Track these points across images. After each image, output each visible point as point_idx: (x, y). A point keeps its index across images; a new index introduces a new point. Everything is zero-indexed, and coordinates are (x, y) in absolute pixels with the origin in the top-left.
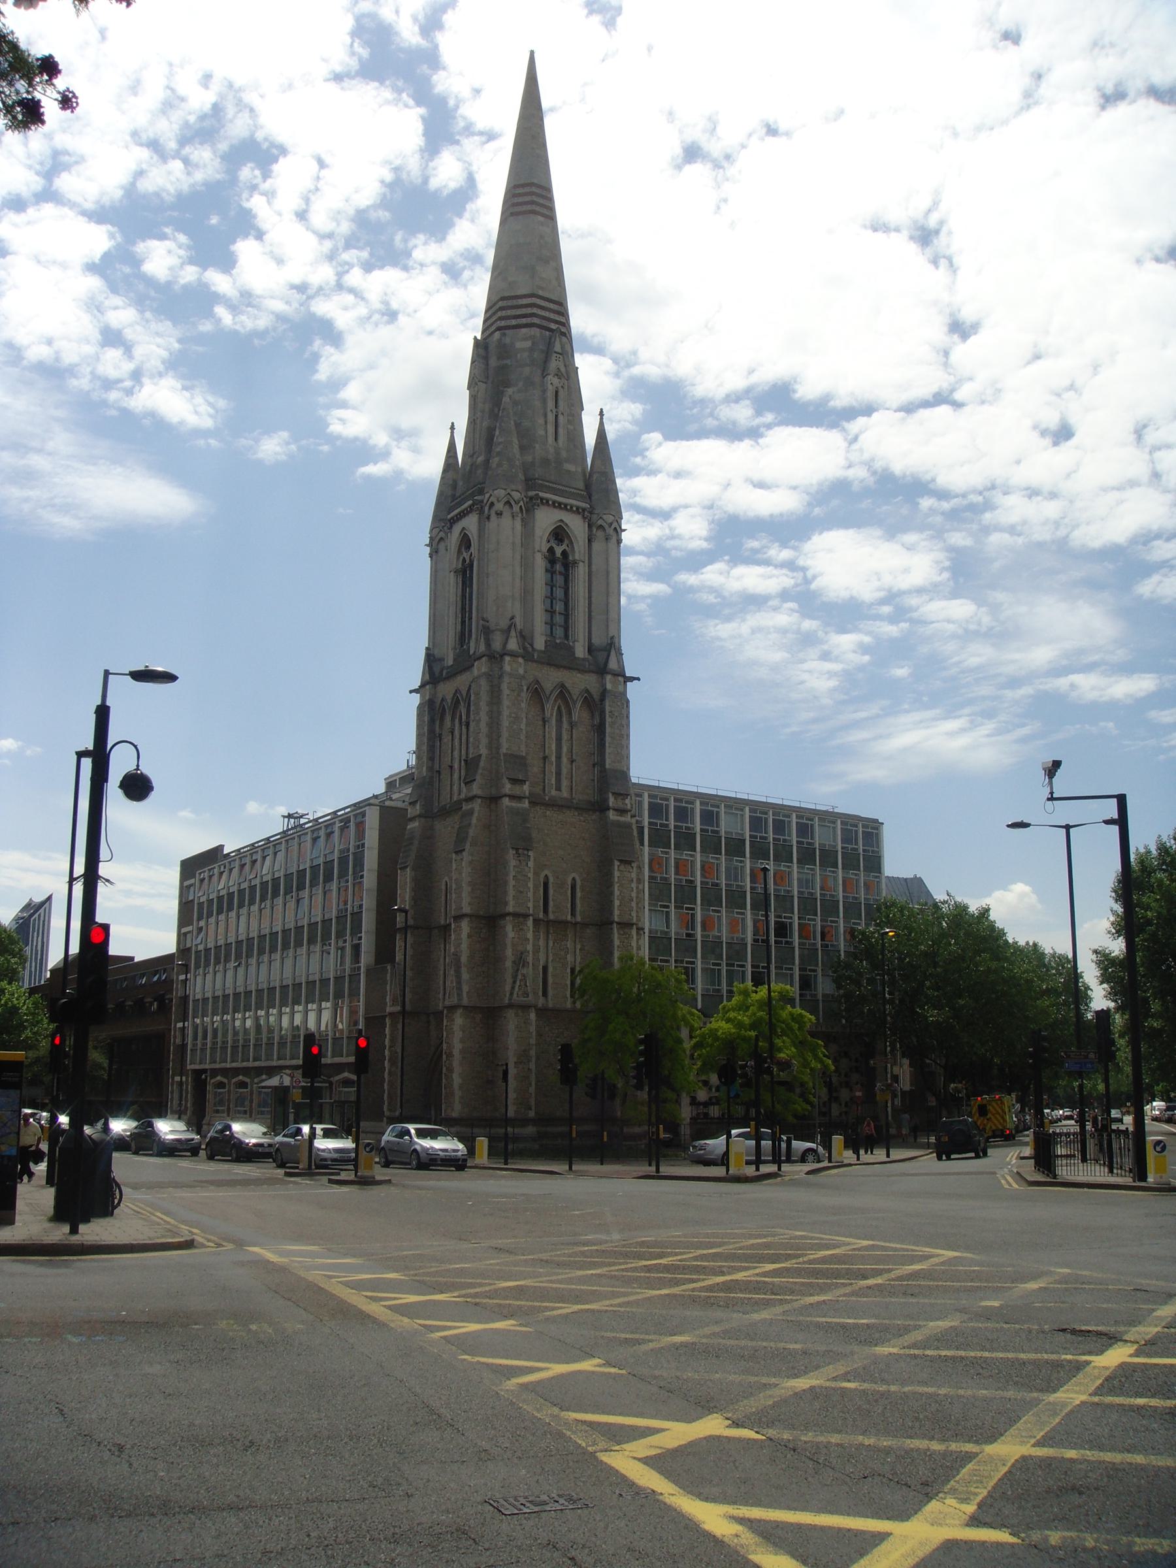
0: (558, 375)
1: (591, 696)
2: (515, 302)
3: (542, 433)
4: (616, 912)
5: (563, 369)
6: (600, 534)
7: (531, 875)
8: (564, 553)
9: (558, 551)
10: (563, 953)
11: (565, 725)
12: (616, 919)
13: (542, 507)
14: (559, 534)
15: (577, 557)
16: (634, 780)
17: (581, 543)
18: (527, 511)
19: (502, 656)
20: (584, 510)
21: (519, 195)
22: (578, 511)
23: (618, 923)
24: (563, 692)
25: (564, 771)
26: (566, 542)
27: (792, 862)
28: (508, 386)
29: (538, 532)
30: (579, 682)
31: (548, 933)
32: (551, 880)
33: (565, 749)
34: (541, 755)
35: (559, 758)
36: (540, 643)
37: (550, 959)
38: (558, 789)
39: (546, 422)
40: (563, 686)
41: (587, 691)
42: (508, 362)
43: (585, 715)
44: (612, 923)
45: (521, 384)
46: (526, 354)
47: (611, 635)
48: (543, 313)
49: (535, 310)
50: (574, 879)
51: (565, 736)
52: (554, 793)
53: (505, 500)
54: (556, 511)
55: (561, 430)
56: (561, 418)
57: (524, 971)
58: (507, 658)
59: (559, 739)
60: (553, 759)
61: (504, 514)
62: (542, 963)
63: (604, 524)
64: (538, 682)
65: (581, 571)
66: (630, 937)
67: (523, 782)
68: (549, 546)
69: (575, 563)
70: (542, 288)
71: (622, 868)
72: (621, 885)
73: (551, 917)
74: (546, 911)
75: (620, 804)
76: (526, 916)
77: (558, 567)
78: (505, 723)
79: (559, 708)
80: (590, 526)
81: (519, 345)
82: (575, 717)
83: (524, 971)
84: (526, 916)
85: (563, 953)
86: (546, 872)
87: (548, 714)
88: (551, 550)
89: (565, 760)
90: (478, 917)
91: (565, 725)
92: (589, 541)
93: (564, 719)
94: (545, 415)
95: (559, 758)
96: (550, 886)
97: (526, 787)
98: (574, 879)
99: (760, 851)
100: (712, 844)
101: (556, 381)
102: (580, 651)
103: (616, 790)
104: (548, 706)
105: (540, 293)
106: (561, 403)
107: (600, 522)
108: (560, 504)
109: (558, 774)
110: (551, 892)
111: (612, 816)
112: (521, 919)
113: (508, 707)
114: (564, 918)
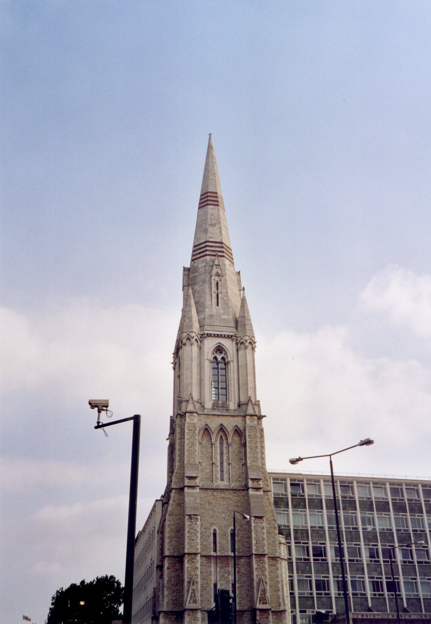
0: (218, 275)
1: (239, 428)
2: (199, 247)
3: (209, 303)
4: (254, 548)
5: (220, 272)
6: (242, 346)
7: (199, 530)
8: (223, 358)
9: (219, 358)
10: (226, 575)
11: (225, 445)
12: (254, 552)
13: (208, 338)
14: (219, 349)
15: (229, 359)
16: (268, 471)
17: (231, 351)
18: (201, 341)
19: (185, 414)
20: (232, 336)
21: (203, 202)
22: (229, 337)
23: (256, 555)
24: (222, 429)
25: (225, 469)
26: (224, 352)
27: (422, 513)
28: (196, 285)
29: (206, 350)
30: (230, 424)
31: (217, 563)
32: (218, 531)
33: (225, 458)
34: (211, 462)
35: (222, 463)
36: (208, 405)
37: (219, 578)
38: (222, 479)
39: (212, 298)
40: (222, 425)
41: (236, 426)
42: (195, 274)
43: (236, 438)
44: (252, 555)
45: (200, 283)
46: (203, 269)
47: (249, 395)
48: (212, 249)
49: (207, 248)
50: (215, 530)
51: (225, 451)
52: (219, 482)
53: (187, 337)
54: (214, 338)
55: (220, 301)
56: (220, 295)
57: (194, 587)
58: (187, 414)
59: (222, 454)
60: (219, 464)
61: (187, 344)
62: (213, 582)
63: (244, 342)
64: (207, 425)
65: (232, 367)
66: (264, 562)
67: (195, 478)
68: (213, 356)
69: (228, 363)
70: (212, 238)
71: (257, 520)
72: (256, 531)
73: (219, 554)
74: (215, 550)
75: (255, 485)
76: (196, 554)
77: (221, 365)
78: (186, 448)
79: (221, 437)
80: (237, 344)
81: (200, 266)
82: (230, 441)
83: (194, 587)
84: (196, 554)
85: (226, 575)
86: (214, 527)
87: (213, 441)
88: (215, 358)
89: (225, 464)
90: (173, 557)
91: (225, 445)
92: (237, 351)
93: (224, 442)
94: (211, 295)
95: (222, 463)
96: (217, 535)
97: (197, 480)
98: (215, 530)
99: (334, 504)
100: (400, 508)
101: (217, 278)
102: (232, 406)
103: (253, 477)
104: (214, 437)
105: (211, 240)
106: (219, 288)
107: (242, 341)
108: (218, 335)
109: (222, 471)
110: (218, 538)
111: (251, 492)
112: (193, 556)
113: (188, 439)
114: (226, 554)
